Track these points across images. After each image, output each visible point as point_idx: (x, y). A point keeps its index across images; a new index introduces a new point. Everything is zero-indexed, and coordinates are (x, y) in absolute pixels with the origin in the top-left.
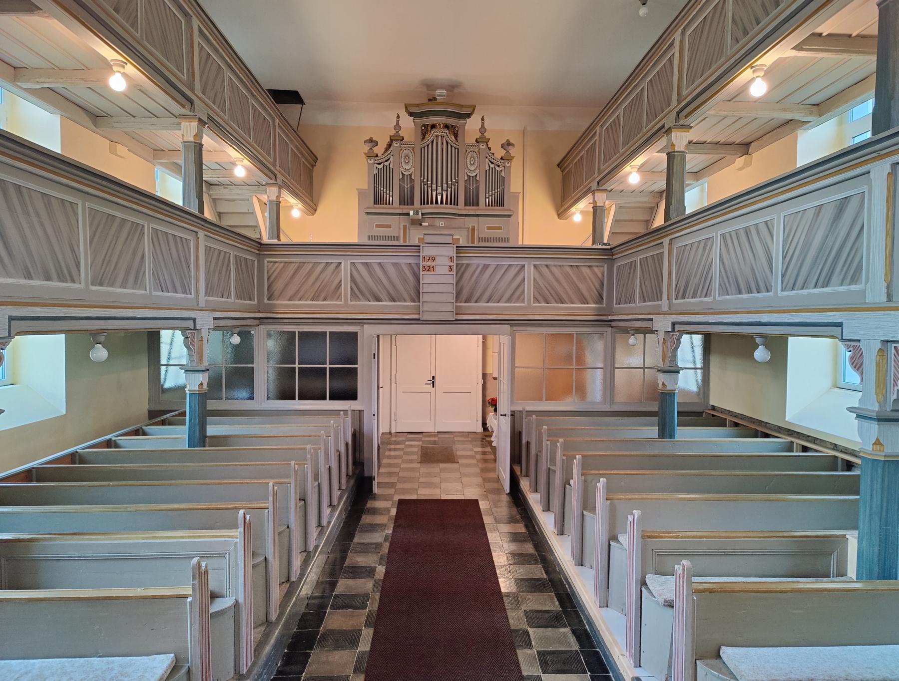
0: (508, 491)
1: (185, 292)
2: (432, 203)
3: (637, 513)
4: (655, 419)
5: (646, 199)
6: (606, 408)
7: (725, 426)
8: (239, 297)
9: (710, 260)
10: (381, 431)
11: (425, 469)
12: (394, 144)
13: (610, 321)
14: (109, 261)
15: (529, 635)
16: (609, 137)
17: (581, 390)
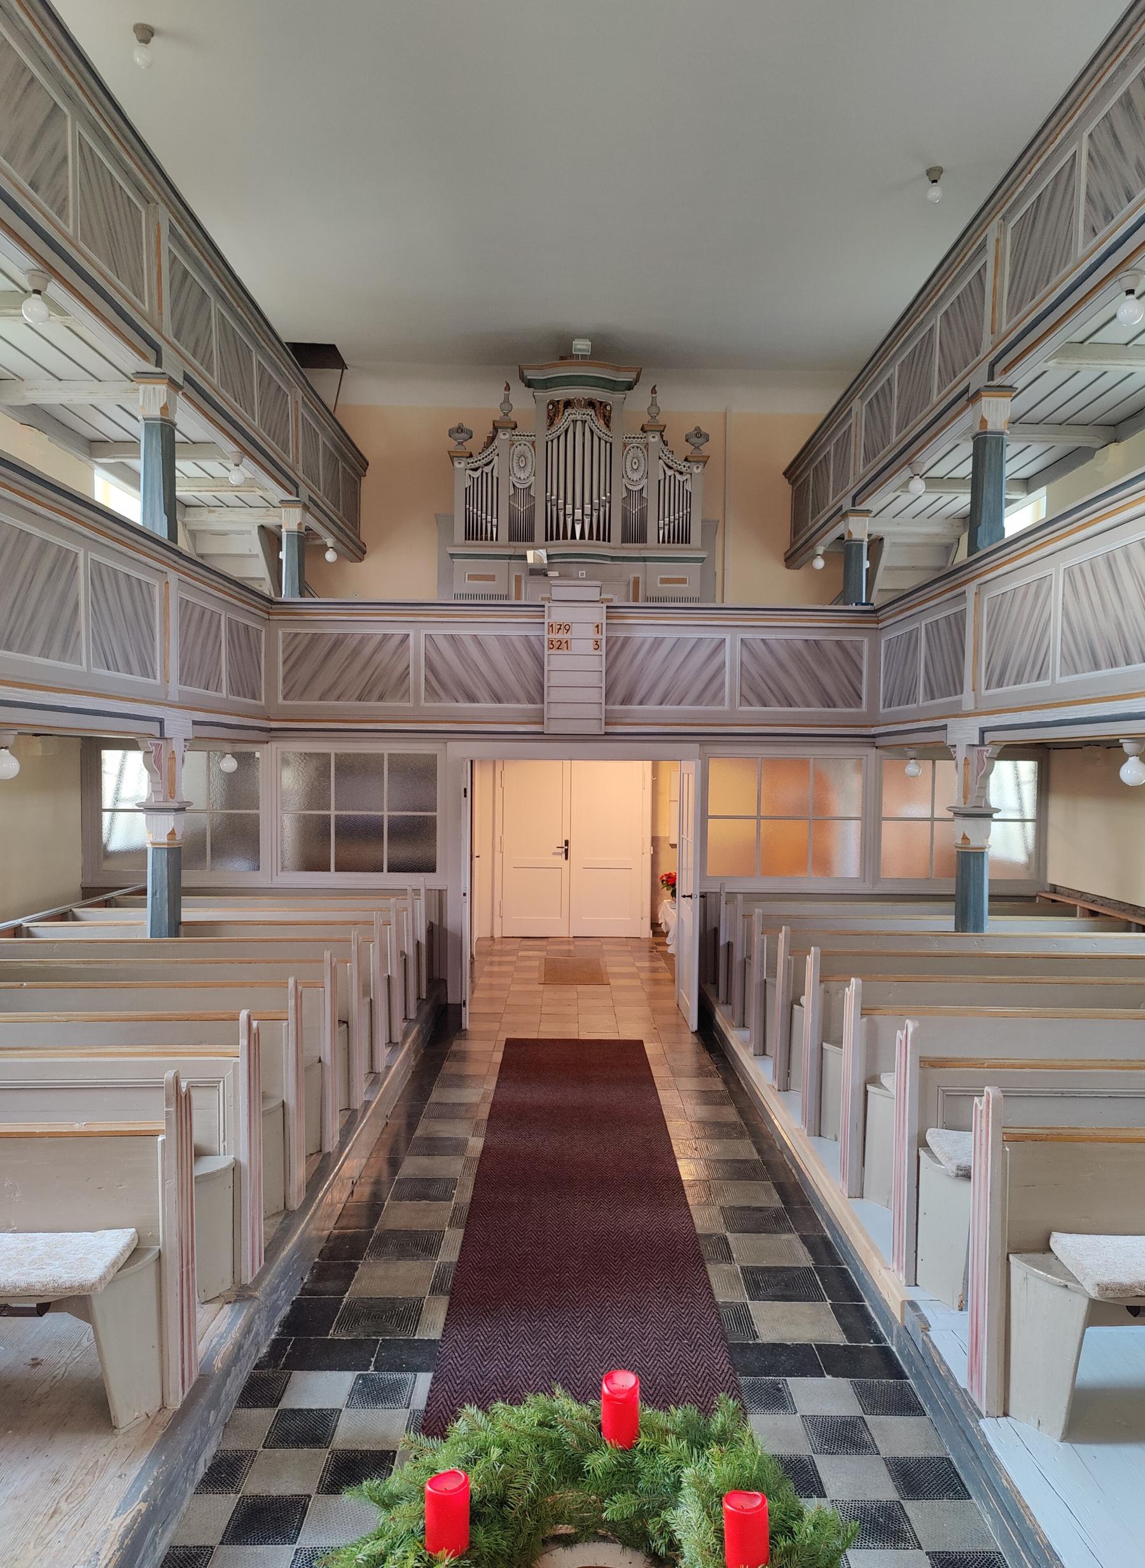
0: (695, 1028)
1: (145, 674)
2: (565, 537)
3: (911, 1025)
4: (951, 906)
5: (936, 529)
6: (866, 888)
7: (1074, 915)
8: (235, 690)
9: (1045, 615)
10: (476, 935)
11: (551, 993)
12: (501, 435)
13: (873, 736)
15: (727, 1244)
16: (874, 418)
17: (823, 862)
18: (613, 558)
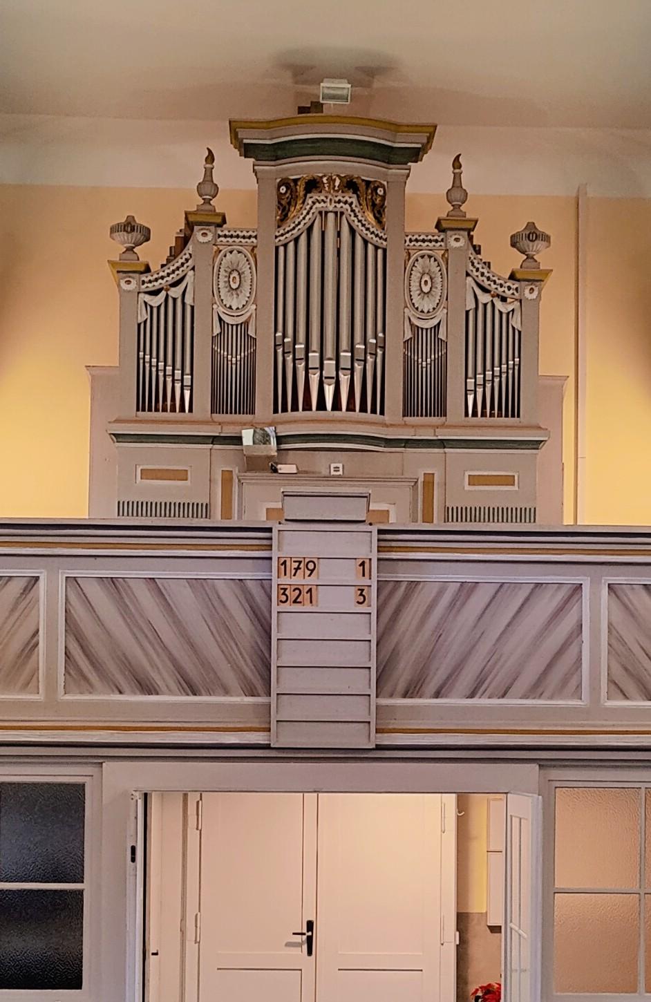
2: (307, 406)
12: (198, 235)
18: (389, 442)
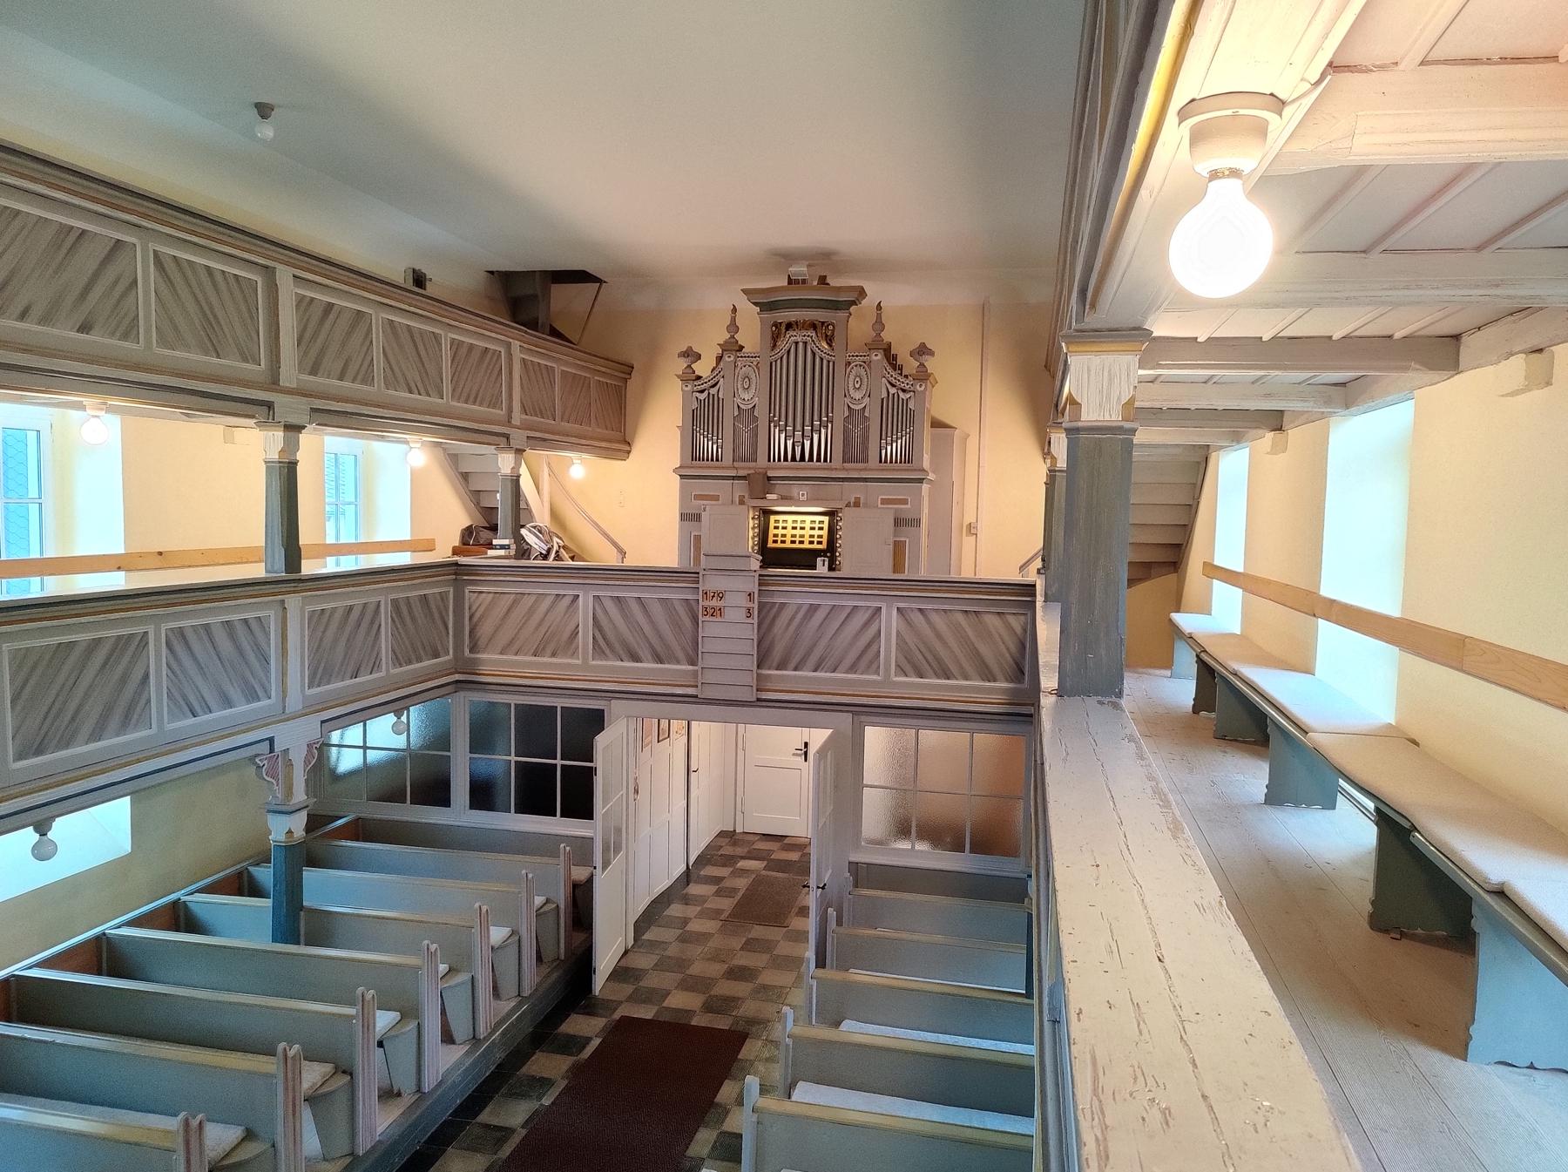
14: (61, 710)
